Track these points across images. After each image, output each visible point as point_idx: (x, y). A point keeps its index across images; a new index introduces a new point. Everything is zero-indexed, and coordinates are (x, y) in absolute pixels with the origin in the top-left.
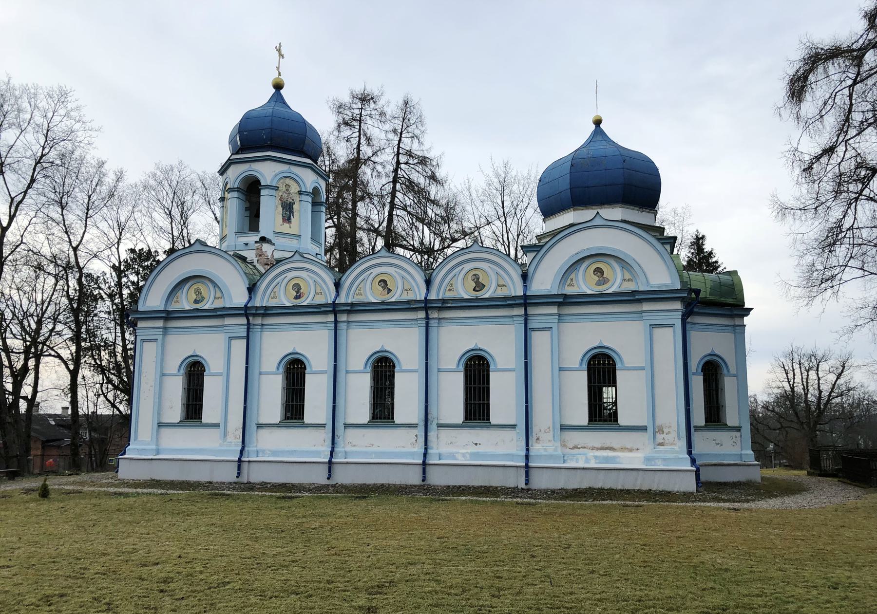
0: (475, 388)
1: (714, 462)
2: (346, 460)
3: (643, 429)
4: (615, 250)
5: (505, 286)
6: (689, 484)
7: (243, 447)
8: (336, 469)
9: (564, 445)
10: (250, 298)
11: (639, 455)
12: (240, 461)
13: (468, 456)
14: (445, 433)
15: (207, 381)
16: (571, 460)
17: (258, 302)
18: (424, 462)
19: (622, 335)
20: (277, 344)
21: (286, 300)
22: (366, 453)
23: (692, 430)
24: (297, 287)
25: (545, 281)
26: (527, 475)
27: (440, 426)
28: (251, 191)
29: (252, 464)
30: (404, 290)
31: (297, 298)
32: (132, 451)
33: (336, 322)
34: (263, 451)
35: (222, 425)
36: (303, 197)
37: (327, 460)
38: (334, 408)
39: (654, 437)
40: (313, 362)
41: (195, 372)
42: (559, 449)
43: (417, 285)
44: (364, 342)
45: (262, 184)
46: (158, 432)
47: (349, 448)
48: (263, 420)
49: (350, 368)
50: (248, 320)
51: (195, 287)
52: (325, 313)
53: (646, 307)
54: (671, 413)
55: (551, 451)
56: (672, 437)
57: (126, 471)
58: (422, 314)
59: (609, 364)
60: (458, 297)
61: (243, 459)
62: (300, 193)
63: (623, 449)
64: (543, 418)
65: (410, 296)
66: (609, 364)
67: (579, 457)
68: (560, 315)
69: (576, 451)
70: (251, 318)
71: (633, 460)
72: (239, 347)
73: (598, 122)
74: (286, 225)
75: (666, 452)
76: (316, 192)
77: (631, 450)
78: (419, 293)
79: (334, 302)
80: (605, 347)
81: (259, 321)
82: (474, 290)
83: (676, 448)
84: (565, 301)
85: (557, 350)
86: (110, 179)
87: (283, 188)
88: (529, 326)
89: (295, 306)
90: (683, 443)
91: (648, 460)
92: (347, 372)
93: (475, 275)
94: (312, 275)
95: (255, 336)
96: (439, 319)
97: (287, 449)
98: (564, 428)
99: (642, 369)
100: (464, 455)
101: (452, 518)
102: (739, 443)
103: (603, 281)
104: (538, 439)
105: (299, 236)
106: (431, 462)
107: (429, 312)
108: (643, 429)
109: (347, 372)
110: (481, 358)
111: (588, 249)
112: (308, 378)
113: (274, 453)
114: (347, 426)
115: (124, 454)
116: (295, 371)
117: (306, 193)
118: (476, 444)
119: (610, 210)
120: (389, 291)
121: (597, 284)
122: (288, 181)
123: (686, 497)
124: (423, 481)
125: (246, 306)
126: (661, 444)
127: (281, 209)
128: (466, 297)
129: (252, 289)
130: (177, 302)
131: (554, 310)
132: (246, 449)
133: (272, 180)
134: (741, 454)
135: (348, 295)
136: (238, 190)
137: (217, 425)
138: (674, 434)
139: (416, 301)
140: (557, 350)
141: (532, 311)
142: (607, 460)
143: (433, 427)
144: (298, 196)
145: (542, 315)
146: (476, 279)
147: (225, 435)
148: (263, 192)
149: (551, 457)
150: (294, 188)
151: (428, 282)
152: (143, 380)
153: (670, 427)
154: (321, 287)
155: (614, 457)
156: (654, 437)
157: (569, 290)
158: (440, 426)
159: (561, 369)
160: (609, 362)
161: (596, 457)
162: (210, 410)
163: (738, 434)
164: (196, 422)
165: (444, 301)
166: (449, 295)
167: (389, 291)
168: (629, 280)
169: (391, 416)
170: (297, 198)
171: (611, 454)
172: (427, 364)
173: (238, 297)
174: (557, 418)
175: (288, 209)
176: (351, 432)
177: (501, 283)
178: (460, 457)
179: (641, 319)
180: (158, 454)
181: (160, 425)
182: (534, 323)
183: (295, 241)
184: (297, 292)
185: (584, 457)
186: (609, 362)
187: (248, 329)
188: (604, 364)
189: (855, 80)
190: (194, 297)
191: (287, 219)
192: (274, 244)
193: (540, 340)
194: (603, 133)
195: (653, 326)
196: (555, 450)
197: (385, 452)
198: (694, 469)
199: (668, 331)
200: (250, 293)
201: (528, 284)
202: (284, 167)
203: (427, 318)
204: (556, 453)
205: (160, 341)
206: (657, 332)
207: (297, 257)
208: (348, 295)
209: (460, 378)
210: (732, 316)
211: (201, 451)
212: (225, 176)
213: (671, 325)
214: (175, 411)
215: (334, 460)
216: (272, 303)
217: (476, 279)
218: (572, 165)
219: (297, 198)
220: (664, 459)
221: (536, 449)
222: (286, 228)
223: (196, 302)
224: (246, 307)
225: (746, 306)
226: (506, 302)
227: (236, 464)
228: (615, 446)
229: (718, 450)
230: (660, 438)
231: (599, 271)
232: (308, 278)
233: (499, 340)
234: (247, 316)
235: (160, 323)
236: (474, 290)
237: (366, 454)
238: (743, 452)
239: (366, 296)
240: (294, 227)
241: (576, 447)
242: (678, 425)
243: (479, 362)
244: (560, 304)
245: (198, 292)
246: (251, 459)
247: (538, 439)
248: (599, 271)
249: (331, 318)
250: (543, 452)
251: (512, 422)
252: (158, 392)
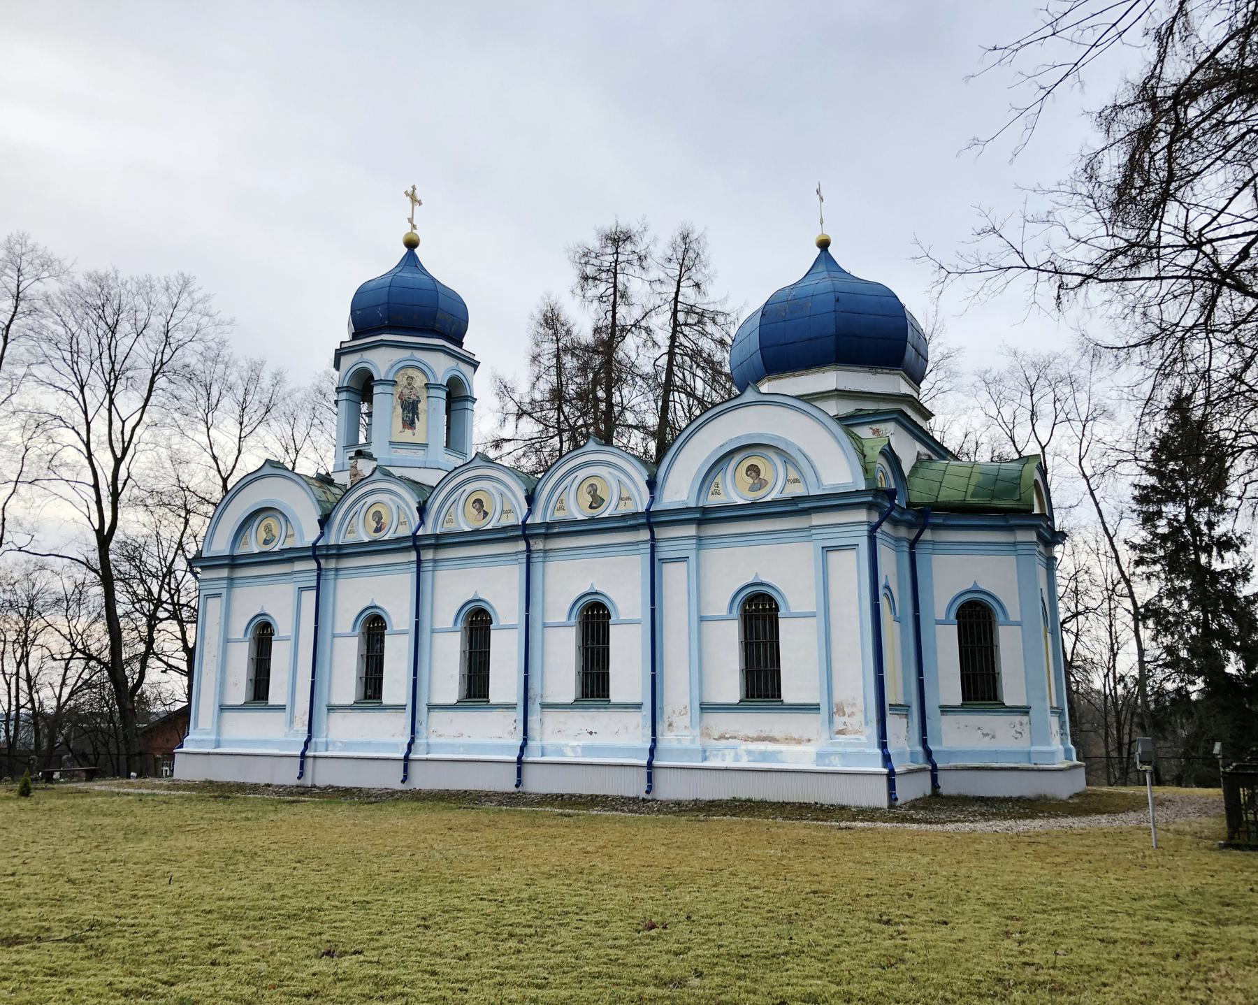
1: (976, 765)
2: (425, 756)
3: (814, 708)
4: (773, 437)
5: (629, 499)
6: (877, 796)
7: (309, 739)
8: (415, 769)
9: (705, 733)
10: (322, 534)
11: (810, 749)
12: (303, 756)
13: (579, 750)
14: (552, 717)
15: (786, 628)
16: (716, 756)
17: (333, 539)
18: (519, 758)
19: (781, 563)
20: (355, 592)
21: (364, 534)
22: (453, 745)
24: (378, 516)
25: (679, 490)
26: (650, 778)
27: (544, 706)
28: (362, 387)
29: (319, 761)
30: (399, 523)
31: (377, 530)
32: (191, 743)
33: (419, 562)
34: (334, 743)
35: (288, 708)
36: (432, 392)
37: (402, 756)
38: (415, 681)
39: (831, 721)
40: (620, 607)
41: (759, 615)
42: (698, 739)
43: (638, 490)
44: (569, 577)
46: (219, 718)
47: (433, 740)
48: (336, 701)
49: (438, 626)
50: (319, 564)
51: (265, 522)
52: (514, 539)
53: (817, 520)
54: (855, 685)
55: (686, 743)
56: (856, 721)
57: (185, 769)
58: (645, 535)
59: (771, 608)
60: (569, 517)
61: (308, 753)
62: (428, 386)
63: (789, 740)
64: (677, 693)
65: (628, 508)
66: (771, 608)
67: (727, 752)
68: (700, 538)
69: (723, 743)
70: (322, 562)
71: (800, 756)
72: (309, 598)
73: (824, 245)
74: (408, 432)
75: (847, 744)
77: (799, 741)
78: (640, 502)
79: (648, 510)
80: (762, 584)
81: (332, 564)
82: (591, 507)
83: (863, 739)
84: (704, 517)
85: (698, 590)
86: (266, 381)
88: (658, 556)
89: (592, 520)
90: (873, 730)
91: (820, 756)
92: (545, 626)
93: (591, 485)
94: (496, 485)
95: (328, 586)
96: (545, 551)
97: (361, 739)
98: (705, 707)
99: (813, 615)
100: (574, 748)
101: (564, 844)
102: (1026, 734)
103: (760, 484)
104: (670, 725)
105: (426, 445)
106: (530, 759)
107: (532, 542)
108: (814, 708)
109: (545, 626)
110: (599, 606)
111: (738, 438)
112: (494, 635)
113: (346, 746)
114: (431, 707)
115: (181, 747)
116: (594, 621)
117: (438, 386)
118: (591, 733)
119: (821, 375)
120: (486, 514)
121: (752, 489)
122: (410, 372)
123: (868, 814)
124: (517, 786)
125: (314, 544)
126: (841, 732)
127: (400, 410)
128: (580, 517)
129: (324, 522)
130: (246, 543)
131: (691, 530)
132: (313, 740)
133: (387, 373)
134: (1029, 753)
135: (436, 523)
136: (348, 389)
137: (281, 708)
138: (859, 717)
139: (635, 515)
140: (698, 590)
141: (661, 533)
142: (764, 756)
143: (535, 708)
144: (424, 391)
145: (676, 538)
146: (593, 490)
147: (291, 722)
148: (376, 390)
149: (686, 752)
150: (420, 380)
151: (531, 499)
152: (206, 648)
153: (854, 705)
154: (629, 489)
155: (774, 753)
156: (831, 721)
157: (713, 500)
158: (544, 706)
159: (702, 619)
160: (770, 605)
161: (749, 752)
162: (796, 679)
163: (1025, 719)
164: (261, 703)
165: (548, 525)
166: (559, 516)
167: (486, 514)
168: (796, 481)
169: (485, 694)
170: (423, 394)
171: (771, 747)
172: (527, 617)
173: (308, 533)
174: (696, 691)
175: (411, 410)
176: (437, 716)
177: (624, 495)
178: (568, 752)
179: (809, 539)
180: (705, 759)
181: (223, 708)
182: (664, 551)
183: (421, 453)
184: (378, 523)
185: (732, 753)
186: (770, 605)
187: (319, 576)
188: (764, 609)
189: (1173, 134)
191: (410, 424)
192: (375, 460)
193: (675, 578)
195: (827, 549)
196: (693, 741)
197: (474, 743)
198: (886, 771)
199: (850, 556)
200: (322, 528)
201: (657, 494)
202: (406, 354)
203: (529, 550)
204: (692, 746)
205: (692, 560)
206: (833, 557)
207: (377, 475)
208: (436, 523)
211: (265, 743)
213: (854, 547)
214: (239, 691)
215: (308, 753)
216: (350, 539)
217: (593, 490)
218: (763, 314)
219: (423, 394)
220: (843, 755)
221: (667, 739)
222: (407, 436)
223: (266, 542)
224: (314, 547)
226: (625, 523)
227: (298, 760)
228: (777, 735)
229: (986, 745)
230: (839, 721)
231: (754, 470)
232: (493, 491)
233: (618, 576)
234: (316, 558)
235: (224, 573)
236: (591, 507)
237: (453, 747)
238: (1034, 748)
239: (727, 494)
240: (419, 433)
241: (722, 737)
242: (865, 698)
244: (700, 522)
245: (268, 529)
246: (317, 754)
247: (670, 725)
248: (754, 470)
249: (413, 556)
250: (675, 745)
251: (638, 701)
252: (827, 646)
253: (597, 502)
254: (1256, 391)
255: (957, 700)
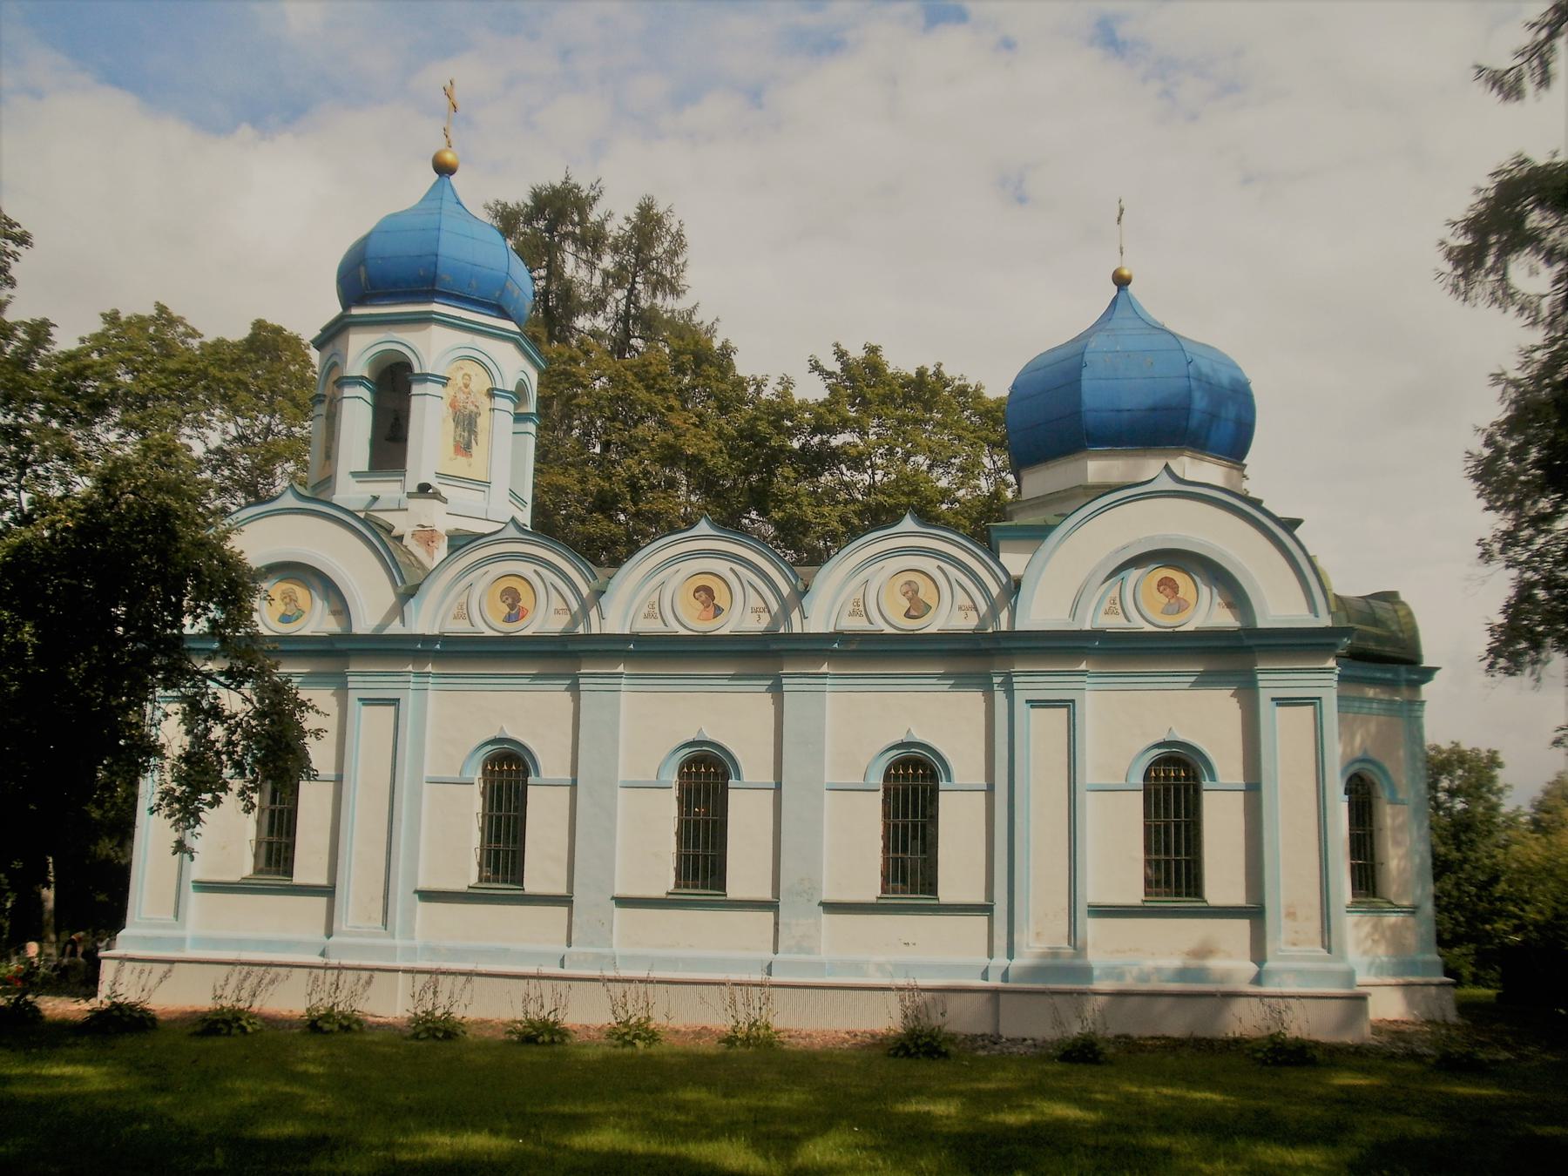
0: (915, 826)
23: (1082, 910)
24: (511, 597)
45: (417, 370)
62: (492, 393)
74: (462, 460)
76: (519, 394)
82: (907, 615)
87: (458, 380)
93: (909, 583)
100: (880, 967)
105: (488, 484)
117: (504, 394)
120: (718, 611)
121: (1165, 612)
144: (486, 400)
167: (718, 611)
169: (930, 886)
184: (512, 607)
190: (282, 608)
194: (1130, 302)
209: (1133, 807)
210: (1391, 685)
211: (289, 945)
212: (329, 349)
219: (485, 403)
220: (1300, 973)
223: (285, 619)
225: (1426, 663)
240: (473, 466)
243: (915, 770)
245: (289, 598)
253: (917, 609)
254: (10, 434)
255: (1133, 892)
